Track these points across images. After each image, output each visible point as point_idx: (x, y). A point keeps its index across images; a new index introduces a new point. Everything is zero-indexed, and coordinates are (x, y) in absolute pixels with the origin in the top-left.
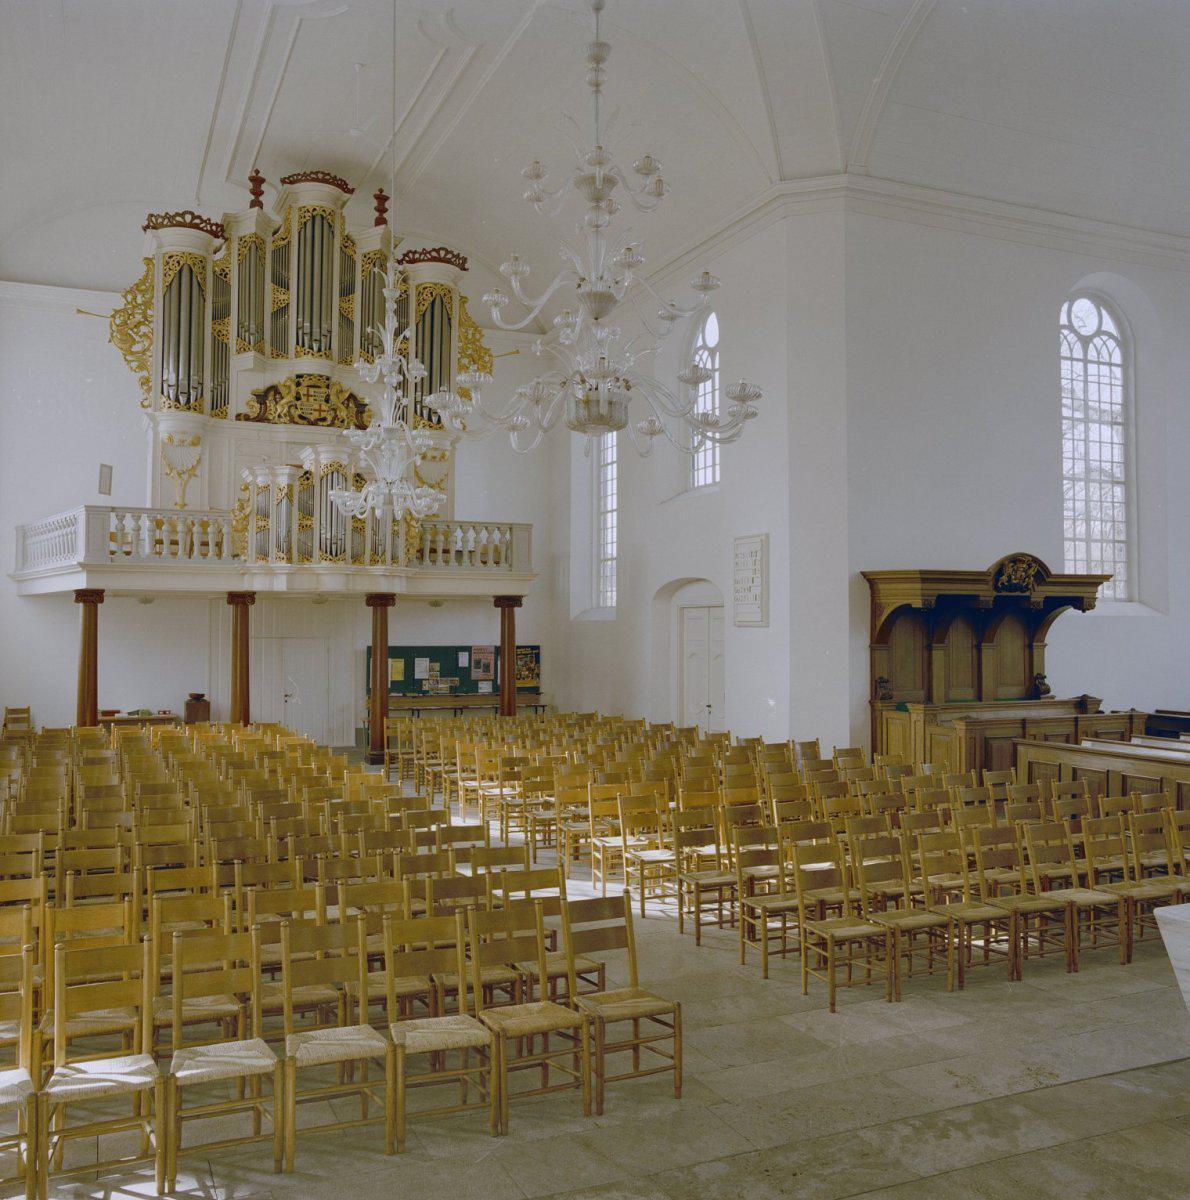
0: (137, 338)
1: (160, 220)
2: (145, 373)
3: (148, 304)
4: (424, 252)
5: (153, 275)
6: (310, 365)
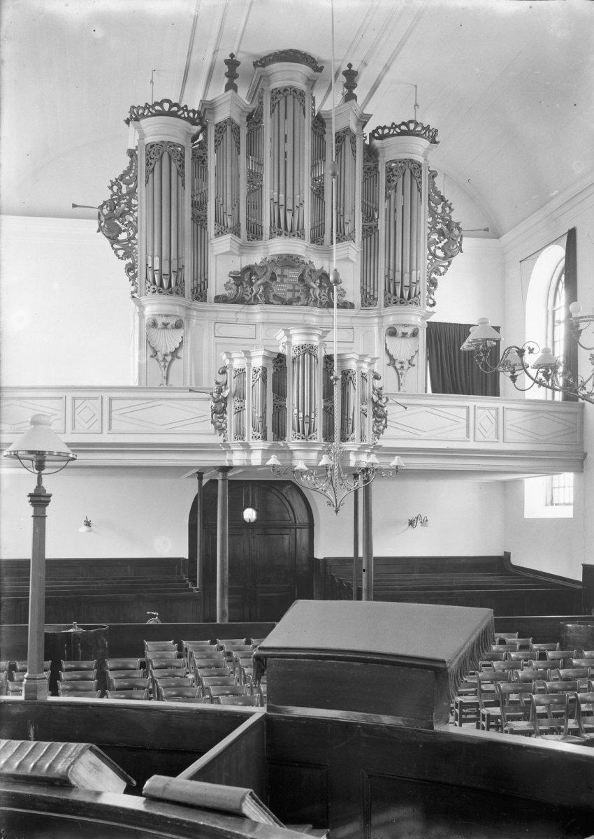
0: (123, 228)
1: (141, 111)
2: (130, 261)
3: (132, 193)
4: (394, 126)
5: (136, 167)
6: (279, 246)
